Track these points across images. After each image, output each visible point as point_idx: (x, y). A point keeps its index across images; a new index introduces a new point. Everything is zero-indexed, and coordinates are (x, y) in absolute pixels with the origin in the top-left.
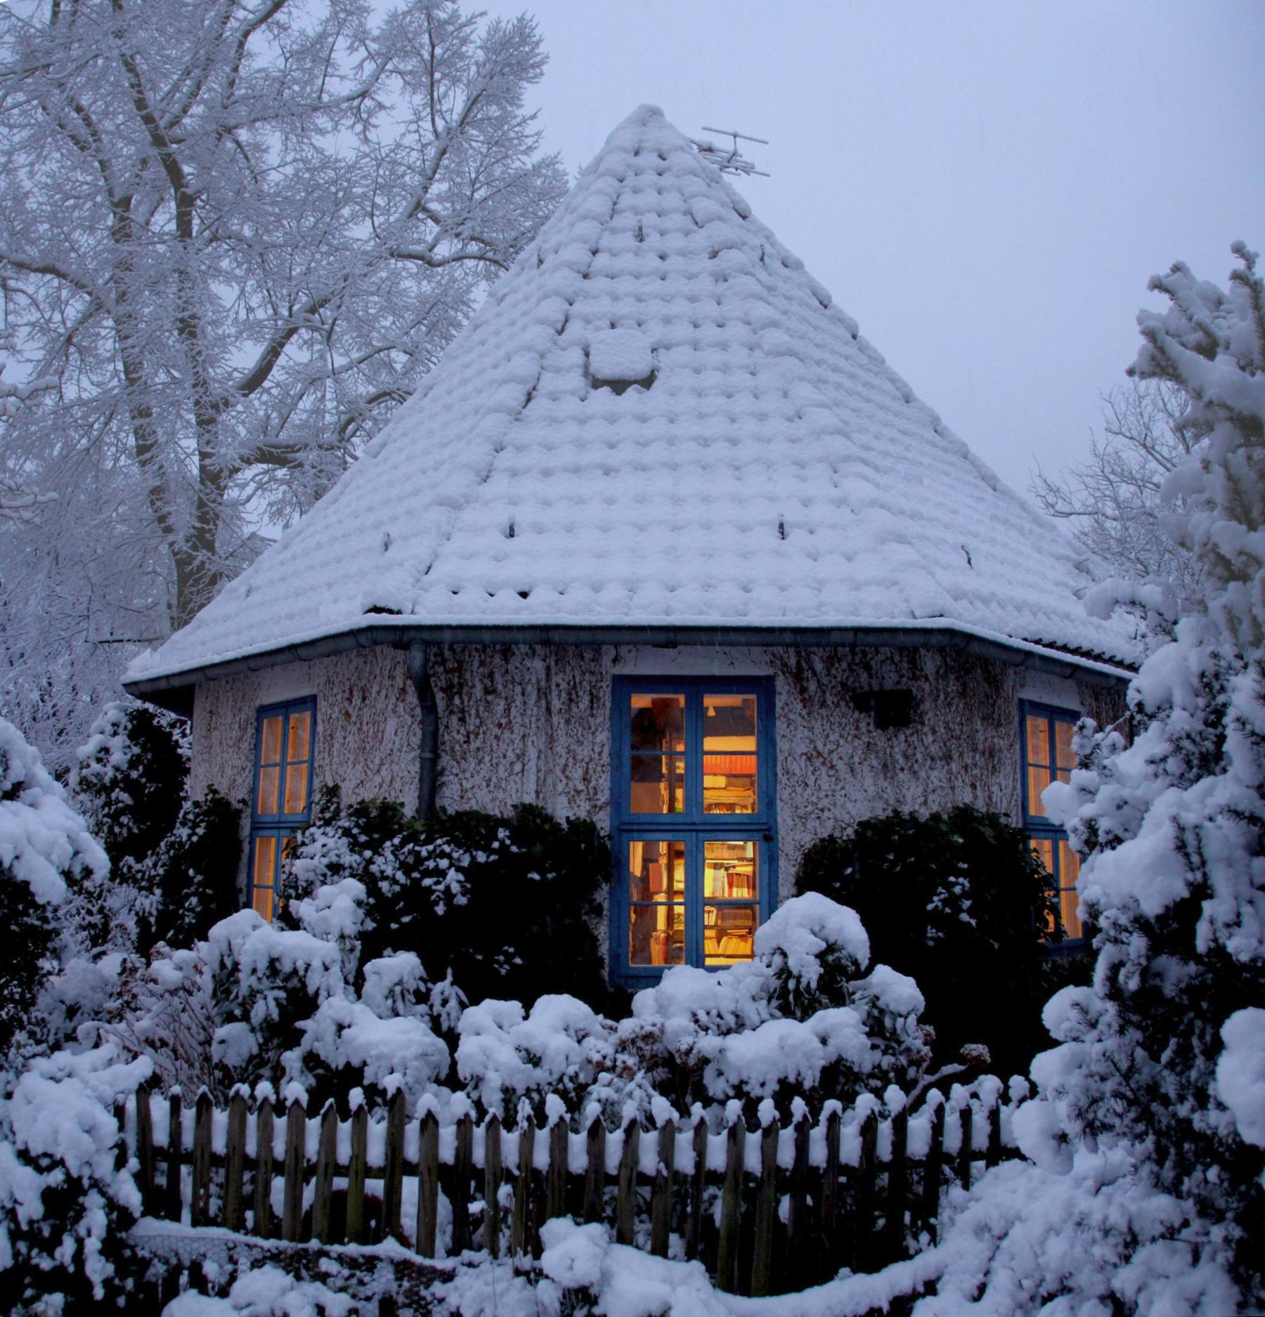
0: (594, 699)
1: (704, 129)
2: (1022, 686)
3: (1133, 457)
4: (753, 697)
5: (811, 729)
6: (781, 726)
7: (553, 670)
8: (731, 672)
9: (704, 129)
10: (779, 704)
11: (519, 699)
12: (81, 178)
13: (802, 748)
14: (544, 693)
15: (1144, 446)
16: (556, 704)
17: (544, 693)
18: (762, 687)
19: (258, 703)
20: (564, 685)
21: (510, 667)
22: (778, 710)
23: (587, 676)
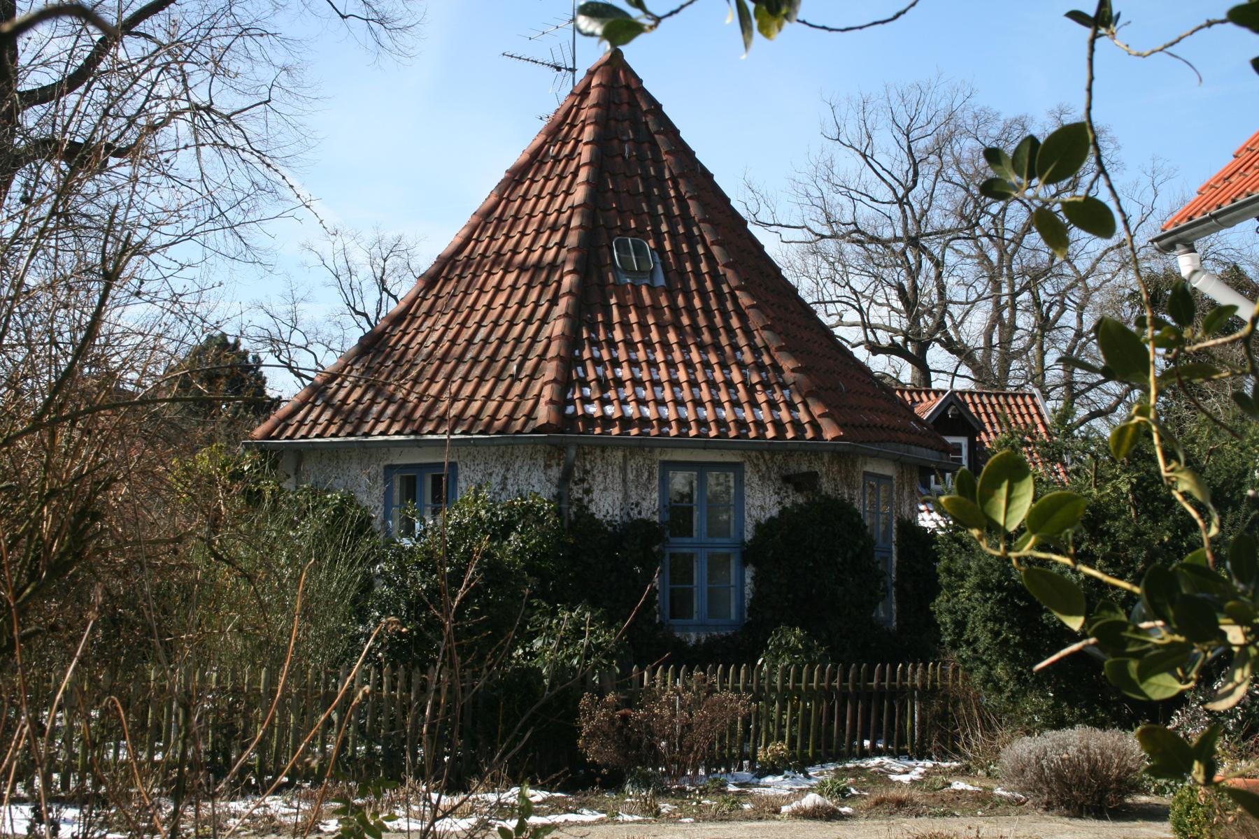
0: (651, 474)
1: (1129, 22)
2: (865, 463)
3: (849, 165)
4: (695, 473)
5: (763, 493)
6: (747, 490)
7: (629, 457)
8: (721, 459)
9: (1129, 22)
10: (746, 478)
11: (610, 474)
12: (85, 278)
13: (758, 503)
14: (623, 470)
15: (864, 156)
16: (631, 476)
17: (623, 470)
18: (737, 467)
19: (388, 462)
20: (634, 466)
21: (606, 455)
22: (746, 482)
23: (647, 461)
